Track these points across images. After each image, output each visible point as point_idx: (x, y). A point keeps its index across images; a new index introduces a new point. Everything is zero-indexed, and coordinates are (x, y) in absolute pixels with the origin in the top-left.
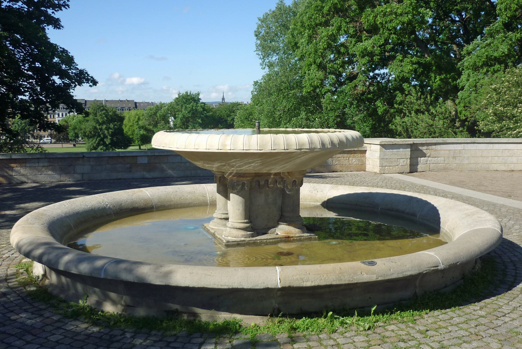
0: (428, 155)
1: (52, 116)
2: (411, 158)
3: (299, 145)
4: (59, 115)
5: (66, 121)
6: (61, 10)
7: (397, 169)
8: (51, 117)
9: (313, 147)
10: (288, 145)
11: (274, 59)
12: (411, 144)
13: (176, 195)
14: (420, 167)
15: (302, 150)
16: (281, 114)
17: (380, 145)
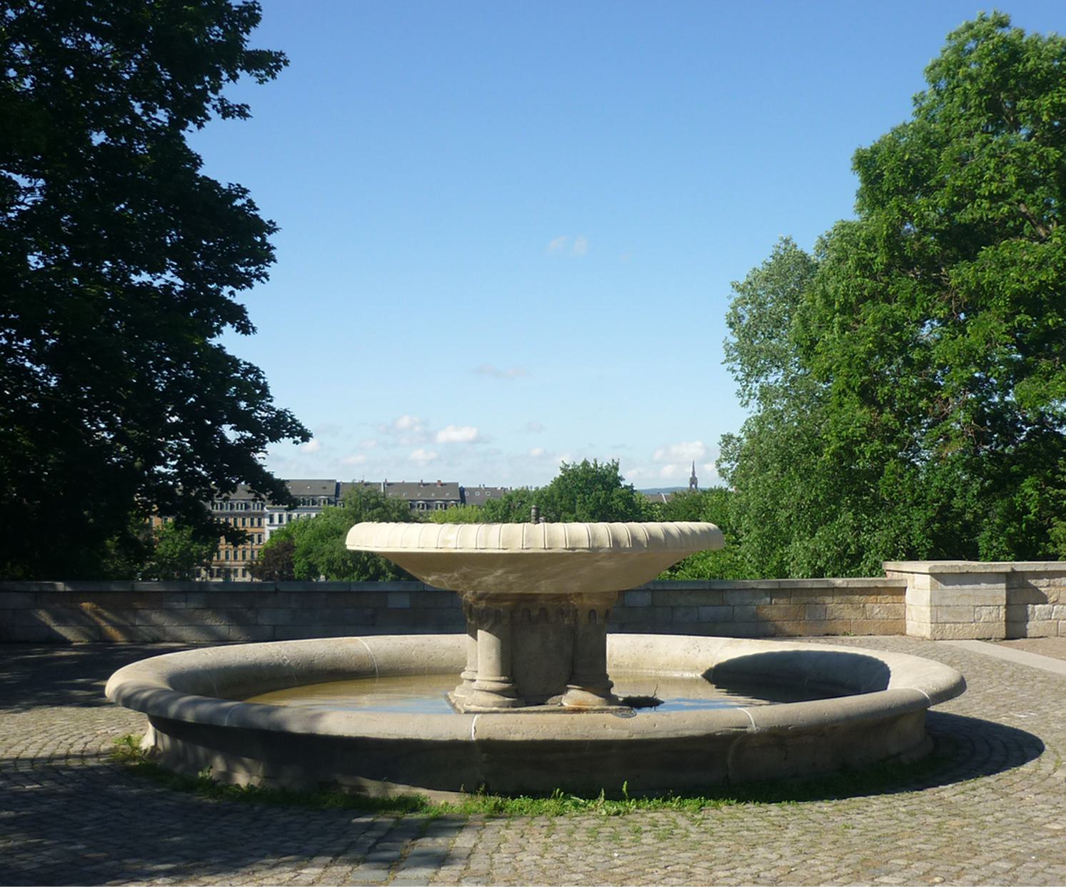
0: (1052, 599)
1: (256, 520)
2: (1008, 605)
3: (570, 541)
4: (272, 520)
5: (288, 535)
6: (251, 286)
7: (974, 629)
8: (252, 523)
9: (596, 545)
10: (550, 541)
11: (772, 379)
12: (1006, 574)
13: (422, 651)
14: (1032, 627)
15: (577, 551)
16: (790, 516)
17: (932, 574)
